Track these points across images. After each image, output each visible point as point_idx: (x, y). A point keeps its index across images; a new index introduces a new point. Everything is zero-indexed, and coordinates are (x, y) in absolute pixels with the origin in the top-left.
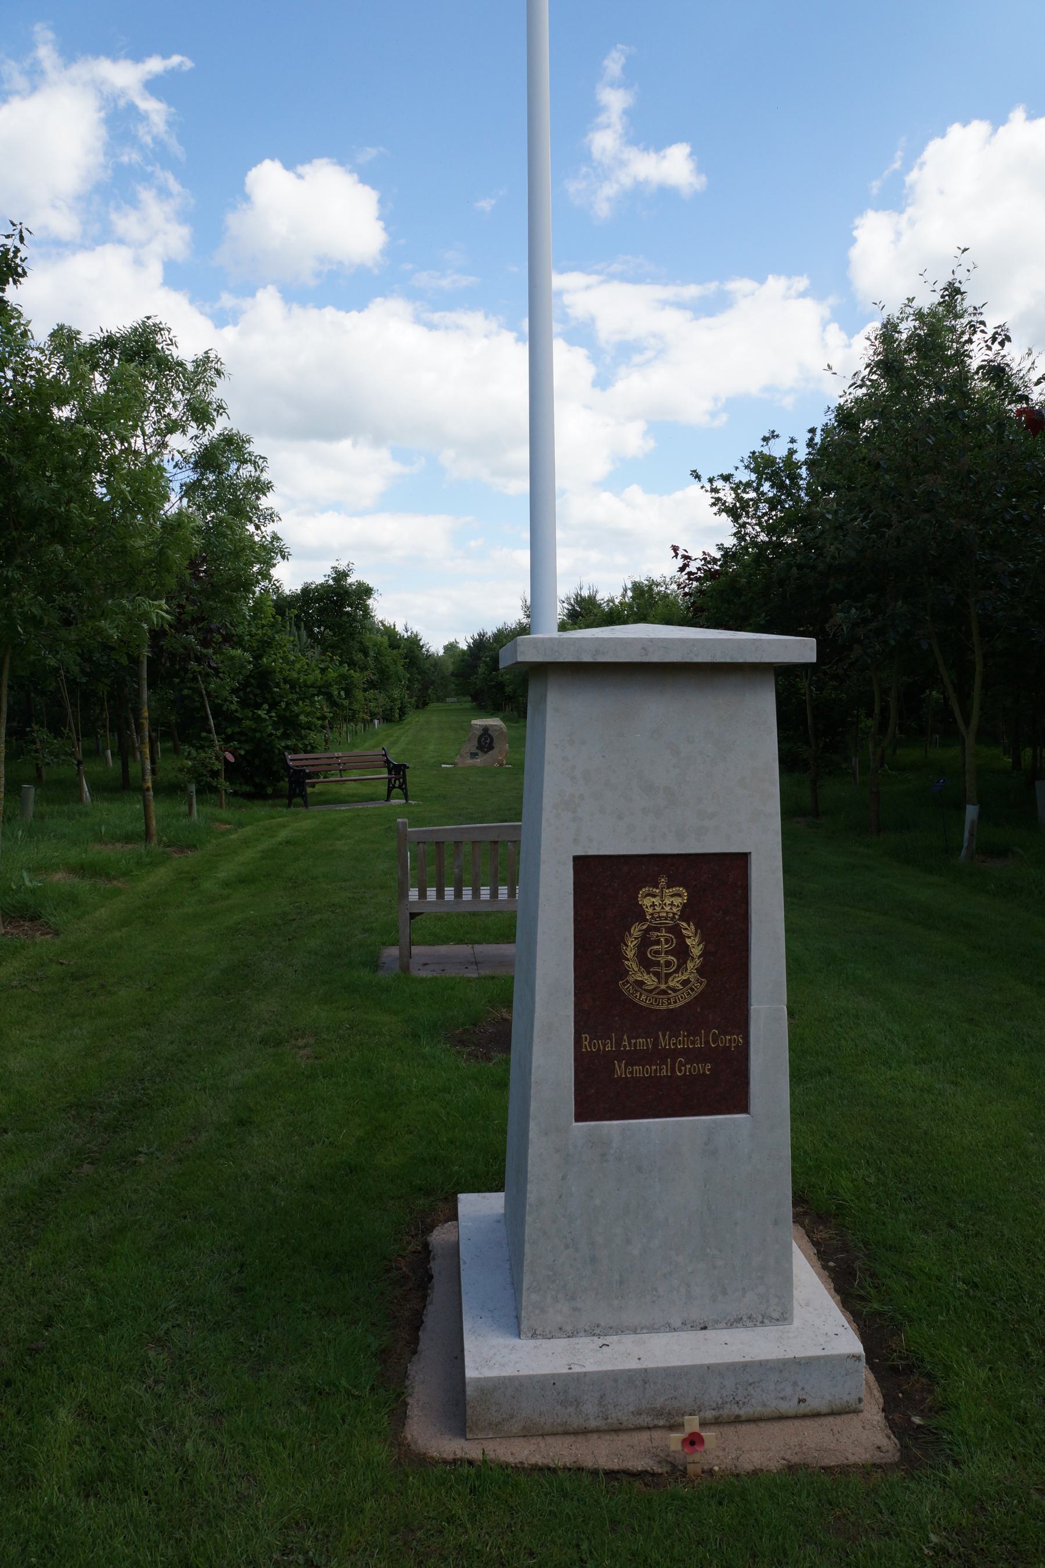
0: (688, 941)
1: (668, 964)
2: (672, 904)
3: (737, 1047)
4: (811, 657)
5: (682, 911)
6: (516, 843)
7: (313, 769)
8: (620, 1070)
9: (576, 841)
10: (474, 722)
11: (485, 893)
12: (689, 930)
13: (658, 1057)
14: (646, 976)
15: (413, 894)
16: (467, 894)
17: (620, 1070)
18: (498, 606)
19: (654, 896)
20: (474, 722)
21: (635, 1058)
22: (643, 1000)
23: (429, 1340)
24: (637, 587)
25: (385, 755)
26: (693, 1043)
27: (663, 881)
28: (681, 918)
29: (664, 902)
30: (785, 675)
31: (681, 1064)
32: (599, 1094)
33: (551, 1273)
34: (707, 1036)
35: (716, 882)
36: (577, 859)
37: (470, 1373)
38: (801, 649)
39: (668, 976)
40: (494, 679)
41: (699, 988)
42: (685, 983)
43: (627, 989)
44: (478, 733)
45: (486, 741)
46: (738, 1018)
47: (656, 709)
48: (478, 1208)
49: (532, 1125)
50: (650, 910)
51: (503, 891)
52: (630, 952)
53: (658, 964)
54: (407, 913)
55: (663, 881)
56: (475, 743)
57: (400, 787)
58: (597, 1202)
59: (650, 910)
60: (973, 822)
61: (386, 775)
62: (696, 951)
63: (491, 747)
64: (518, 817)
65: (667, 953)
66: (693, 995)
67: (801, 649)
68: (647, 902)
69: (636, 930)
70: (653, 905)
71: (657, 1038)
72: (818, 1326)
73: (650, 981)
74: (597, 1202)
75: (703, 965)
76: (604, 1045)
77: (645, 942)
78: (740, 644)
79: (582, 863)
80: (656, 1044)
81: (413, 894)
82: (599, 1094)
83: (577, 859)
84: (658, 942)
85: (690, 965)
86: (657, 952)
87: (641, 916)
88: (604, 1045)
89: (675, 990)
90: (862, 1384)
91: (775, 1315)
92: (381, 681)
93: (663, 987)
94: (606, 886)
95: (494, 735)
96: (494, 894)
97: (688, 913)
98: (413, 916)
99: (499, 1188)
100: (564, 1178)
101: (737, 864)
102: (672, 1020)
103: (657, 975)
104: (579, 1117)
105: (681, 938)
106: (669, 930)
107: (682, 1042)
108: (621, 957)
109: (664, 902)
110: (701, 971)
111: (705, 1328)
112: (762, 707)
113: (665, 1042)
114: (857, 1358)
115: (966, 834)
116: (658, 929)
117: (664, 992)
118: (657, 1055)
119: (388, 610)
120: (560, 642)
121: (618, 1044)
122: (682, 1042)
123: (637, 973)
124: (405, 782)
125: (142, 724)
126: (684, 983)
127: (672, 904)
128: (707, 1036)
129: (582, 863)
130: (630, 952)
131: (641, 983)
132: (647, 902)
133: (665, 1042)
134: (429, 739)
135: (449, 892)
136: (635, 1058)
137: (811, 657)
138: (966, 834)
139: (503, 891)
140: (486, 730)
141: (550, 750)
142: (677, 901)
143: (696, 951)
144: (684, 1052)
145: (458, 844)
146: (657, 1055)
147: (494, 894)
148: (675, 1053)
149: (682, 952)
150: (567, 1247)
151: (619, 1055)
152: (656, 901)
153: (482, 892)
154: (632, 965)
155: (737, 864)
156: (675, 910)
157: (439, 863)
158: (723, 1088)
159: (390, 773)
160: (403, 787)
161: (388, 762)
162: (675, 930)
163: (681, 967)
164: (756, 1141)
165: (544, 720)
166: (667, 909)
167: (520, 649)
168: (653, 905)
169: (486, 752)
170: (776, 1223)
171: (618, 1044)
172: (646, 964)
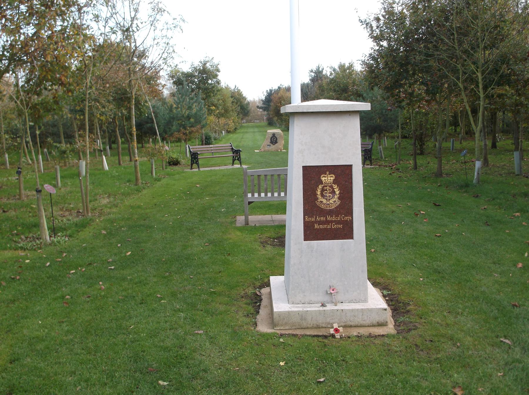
8: (316, 226)
9: (303, 162)
10: (268, 131)
11: (276, 194)
12: (335, 186)
15: (250, 195)
16: (269, 195)
17: (316, 226)
20: (268, 131)
21: (320, 223)
22: (323, 206)
27: (328, 173)
32: (311, 233)
35: (343, 173)
36: (303, 167)
37: (275, 310)
38: (365, 106)
39: (329, 200)
40: (275, 110)
43: (318, 204)
44: (271, 136)
45: (274, 140)
46: (350, 212)
47: (325, 124)
48: (275, 280)
49: (292, 242)
51: (282, 194)
55: (328, 173)
57: (238, 160)
60: (479, 169)
63: (276, 142)
67: (365, 106)
68: (323, 179)
69: (320, 187)
72: (375, 300)
73: (324, 201)
74: (310, 264)
77: (323, 190)
78: (348, 105)
79: (305, 168)
81: (250, 195)
82: (311, 233)
83: (303, 167)
85: (336, 197)
86: (326, 193)
87: (321, 183)
90: (388, 316)
91: (363, 299)
92: (225, 113)
94: (312, 175)
95: (278, 137)
97: (335, 182)
98: (250, 203)
101: (349, 167)
102: (330, 212)
103: (326, 199)
104: (305, 239)
105: (333, 189)
107: (334, 218)
108: (316, 194)
109: (328, 179)
110: (339, 198)
116: (326, 186)
118: (327, 222)
119: (227, 80)
121: (316, 219)
122: (334, 218)
123: (320, 199)
125: (133, 134)
129: (305, 168)
131: (322, 202)
132: (323, 179)
133: (329, 218)
134: (253, 138)
135: (263, 195)
136: (320, 223)
138: (476, 174)
140: (274, 135)
142: (332, 178)
143: (337, 193)
144: (334, 221)
145: (266, 176)
146: (327, 222)
148: (332, 222)
149: (333, 192)
151: (316, 222)
152: (326, 178)
154: (319, 196)
155: (349, 167)
158: (347, 232)
159: (233, 153)
161: (232, 149)
162: (331, 187)
163: (333, 197)
169: (274, 145)
170: (362, 272)
171: (316, 219)
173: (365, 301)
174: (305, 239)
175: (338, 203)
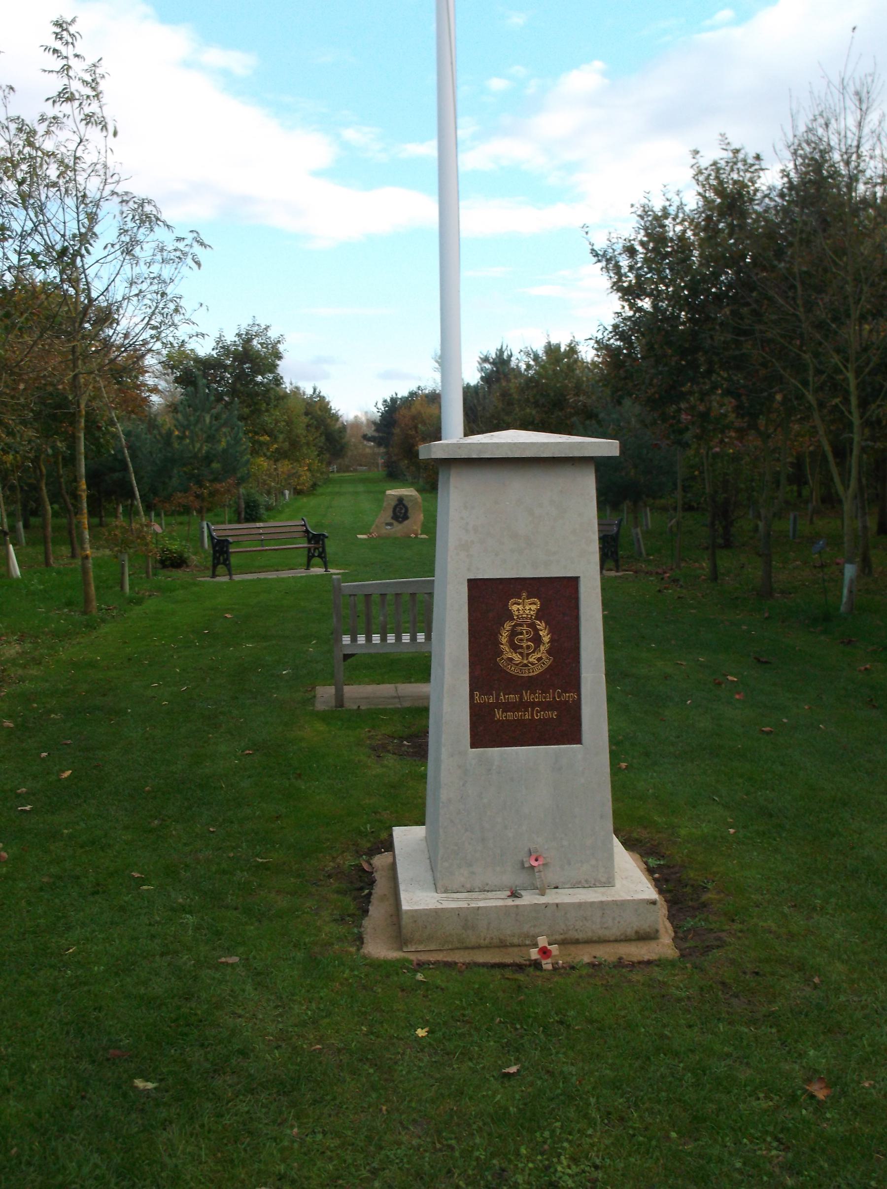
0: (541, 633)
1: (528, 647)
2: (530, 609)
3: (573, 701)
4: (616, 452)
5: (537, 614)
6: (431, 594)
7: (236, 539)
8: (499, 715)
9: (469, 570)
10: (389, 492)
11: (406, 638)
12: (541, 625)
13: (522, 708)
14: (514, 655)
15: (346, 639)
18: (411, 371)
19: (519, 604)
21: (508, 707)
22: (513, 670)
23: (381, 887)
24: (552, 350)
25: (304, 525)
26: (545, 698)
27: (524, 595)
28: (536, 619)
29: (525, 608)
30: (600, 465)
31: (538, 712)
32: (486, 731)
33: (456, 848)
34: (554, 694)
35: (558, 595)
36: (470, 581)
37: (405, 906)
39: (528, 655)
41: (548, 663)
42: (539, 659)
43: (502, 663)
44: (393, 503)
45: (401, 511)
46: (573, 683)
47: (519, 487)
48: (406, 837)
50: (516, 613)
51: (421, 637)
52: (504, 640)
53: (521, 647)
54: (342, 656)
55: (524, 595)
56: (390, 513)
57: (320, 556)
58: (485, 801)
59: (516, 613)
60: (851, 581)
61: (306, 545)
62: (546, 639)
63: (405, 517)
64: (432, 573)
65: (528, 640)
66: (545, 667)
68: (515, 608)
69: (508, 626)
70: (518, 610)
71: (522, 695)
72: (631, 881)
73: (517, 658)
74: (485, 801)
75: (550, 648)
76: (489, 699)
77: (513, 633)
80: (521, 698)
82: (486, 731)
83: (470, 581)
84: (522, 634)
85: (542, 648)
86: (521, 640)
87: (510, 617)
88: (489, 699)
89: (533, 664)
90: (660, 918)
91: (603, 880)
92: (291, 451)
93: (525, 662)
94: (489, 599)
96: (414, 638)
97: (540, 615)
98: (346, 657)
99: (423, 824)
100: (463, 785)
101: (573, 583)
102: (532, 683)
103: (521, 654)
104: (473, 745)
105: (537, 631)
106: (529, 626)
107: (538, 697)
109: (525, 608)
110: (549, 652)
111: (557, 888)
112: (587, 486)
113: (527, 697)
114: (654, 903)
115: (845, 591)
116: (521, 625)
117: (526, 665)
120: (459, 446)
121: (497, 698)
122: (538, 697)
123: (508, 652)
124: (324, 550)
125: (81, 496)
126: (538, 660)
127: (530, 609)
128: (554, 694)
130: (504, 640)
131: (511, 660)
132: (515, 608)
133: (527, 697)
134: (354, 508)
136: (508, 707)
137: (616, 452)
138: (845, 591)
139: (421, 637)
140: (400, 500)
141: (452, 512)
142: (533, 607)
143: (546, 639)
144: (539, 704)
147: (414, 638)
148: (533, 705)
149: (537, 640)
150: (466, 830)
151: (497, 705)
153: (403, 638)
154: (505, 648)
155: (573, 583)
156: (532, 613)
157: (365, 614)
158: (566, 729)
160: (322, 555)
161: (307, 531)
162: (532, 626)
164: (589, 757)
165: (448, 493)
166: (527, 612)
167: (434, 450)
168: (518, 610)
169: (400, 522)
170: (602, 817)
171: (497, 698)
172: (514, 647)
173: (609, 883)
174: (473, 745)
175: (548, 661)
